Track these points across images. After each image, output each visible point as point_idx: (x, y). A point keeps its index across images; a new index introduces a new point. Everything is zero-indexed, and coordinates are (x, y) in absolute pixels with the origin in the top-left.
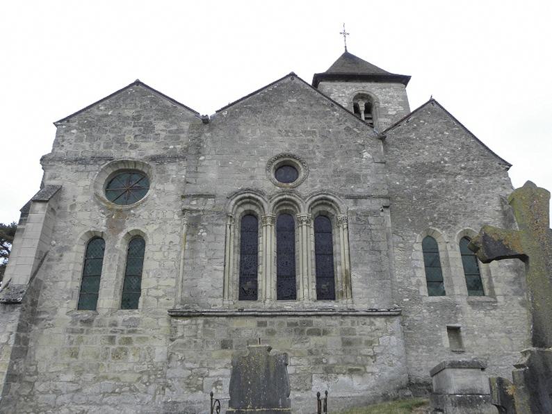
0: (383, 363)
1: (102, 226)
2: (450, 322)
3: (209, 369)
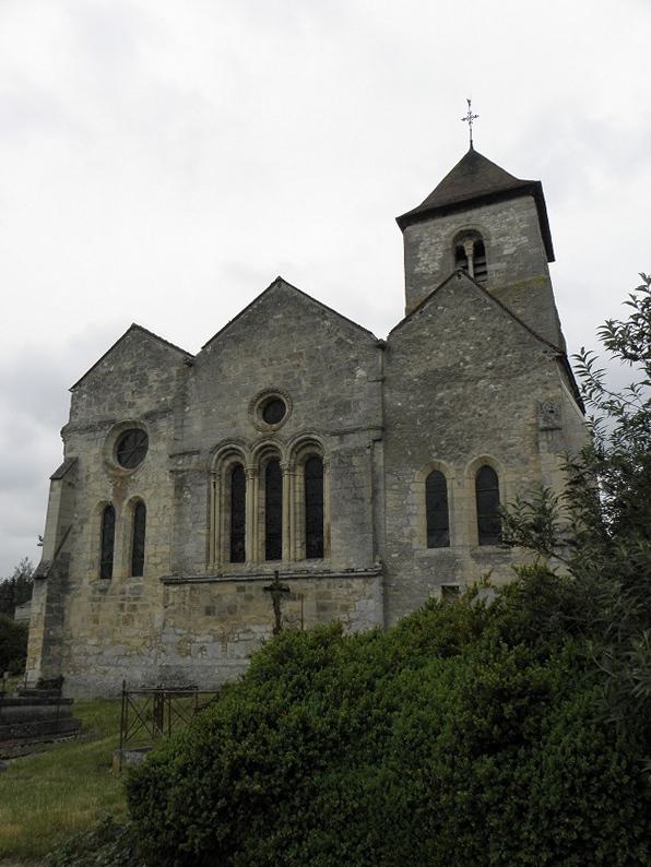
3: (196, 635)
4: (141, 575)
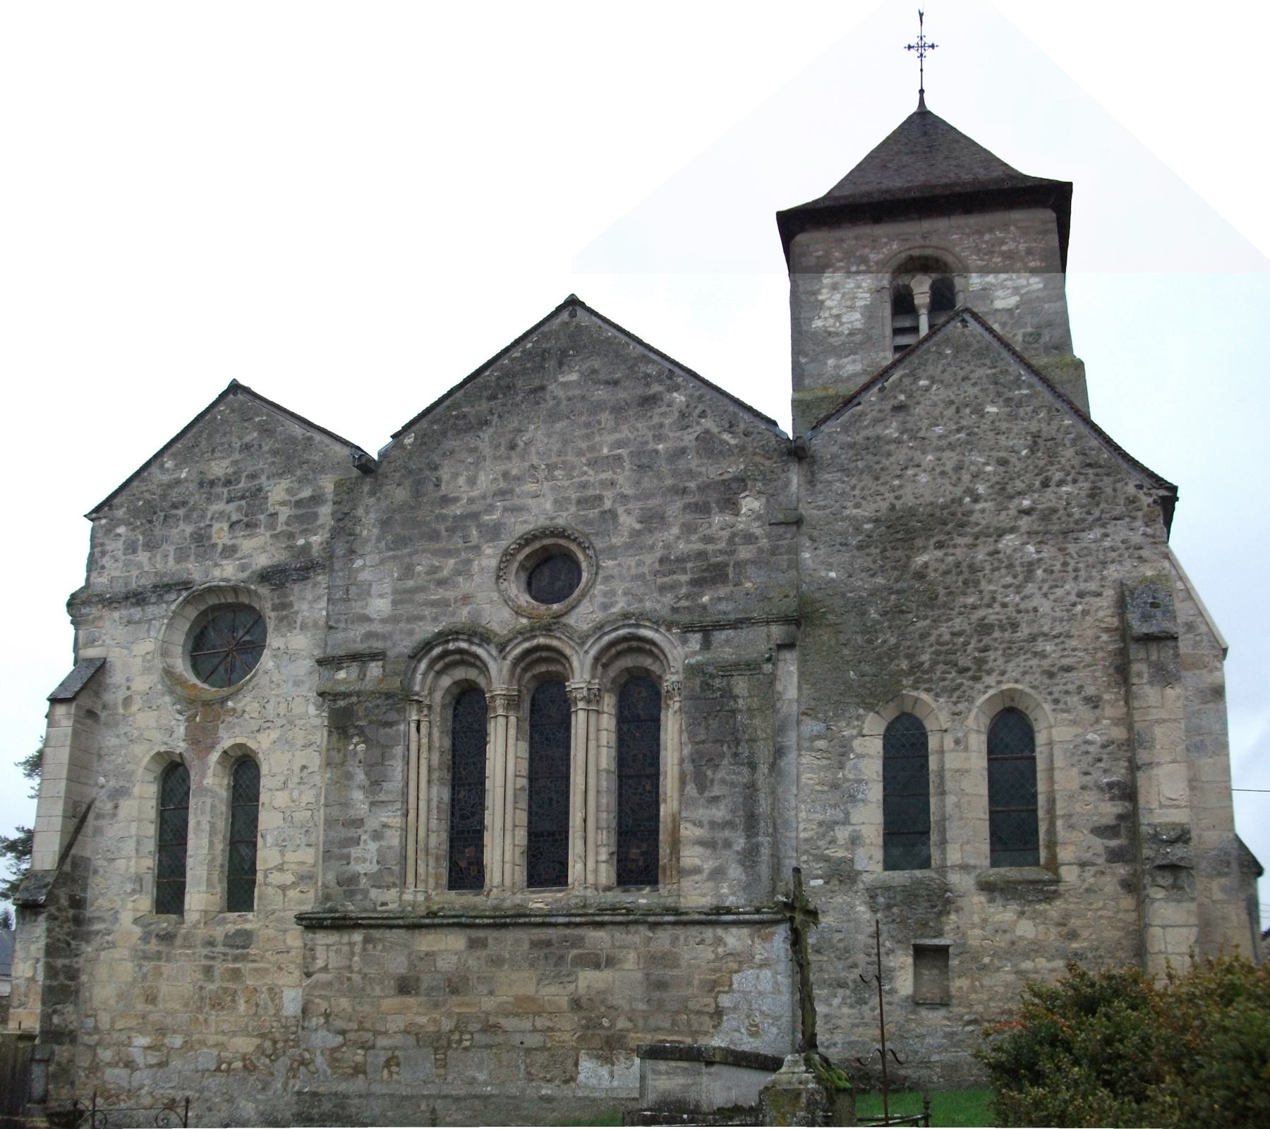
0: (738, 1030)
2: (922, 936)
4: (250, 907)
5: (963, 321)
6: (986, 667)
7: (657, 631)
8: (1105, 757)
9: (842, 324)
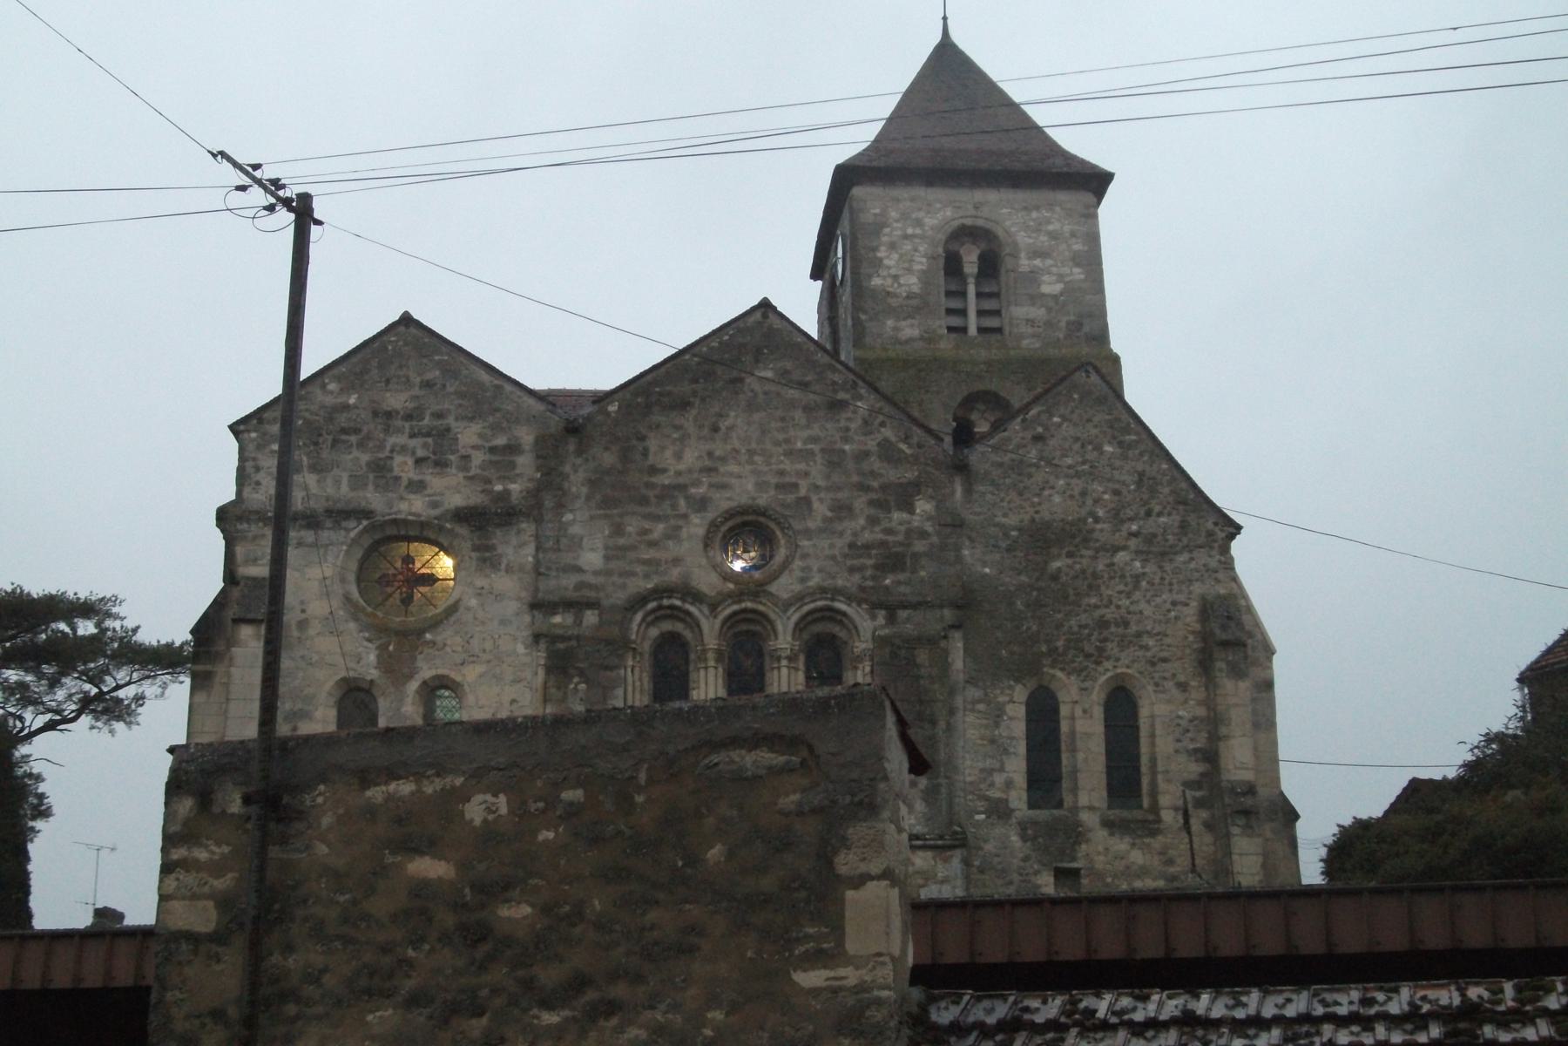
1: (368, 665)
2: (1062, 861)
5: (1087, 371)
6: (1105, 654)
7: (849, 605)
8: (1191, 728)
9: (900, 285)
